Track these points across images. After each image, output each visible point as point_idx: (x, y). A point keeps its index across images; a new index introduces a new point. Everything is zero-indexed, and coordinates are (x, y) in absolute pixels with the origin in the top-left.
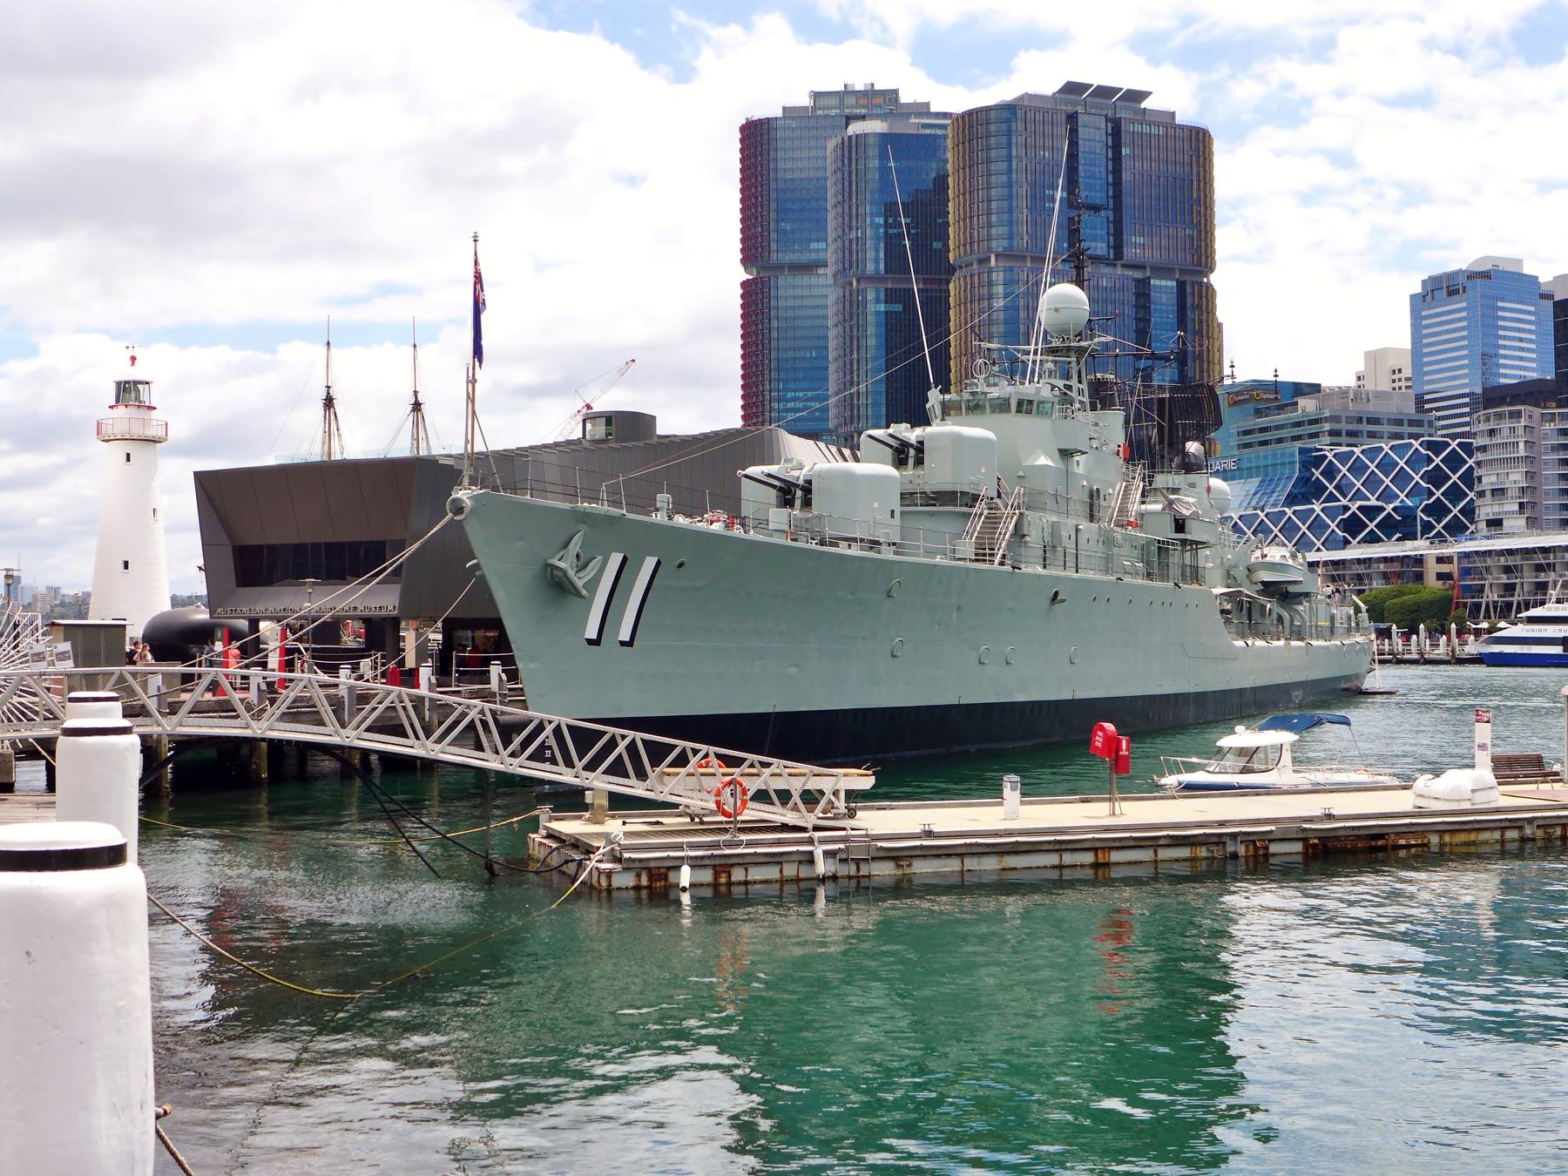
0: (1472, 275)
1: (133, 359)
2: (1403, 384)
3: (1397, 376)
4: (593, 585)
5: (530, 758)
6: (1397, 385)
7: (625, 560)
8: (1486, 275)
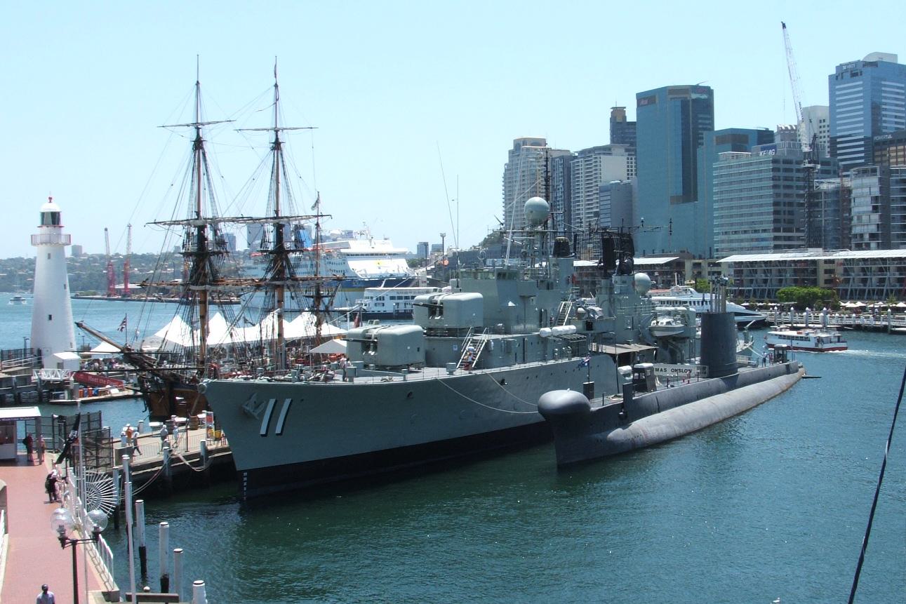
0: (866, 64)
2: (826, 129)
3: (822, 124)
4: (262, 415)
6: (822, 129)
8: (873, 64)
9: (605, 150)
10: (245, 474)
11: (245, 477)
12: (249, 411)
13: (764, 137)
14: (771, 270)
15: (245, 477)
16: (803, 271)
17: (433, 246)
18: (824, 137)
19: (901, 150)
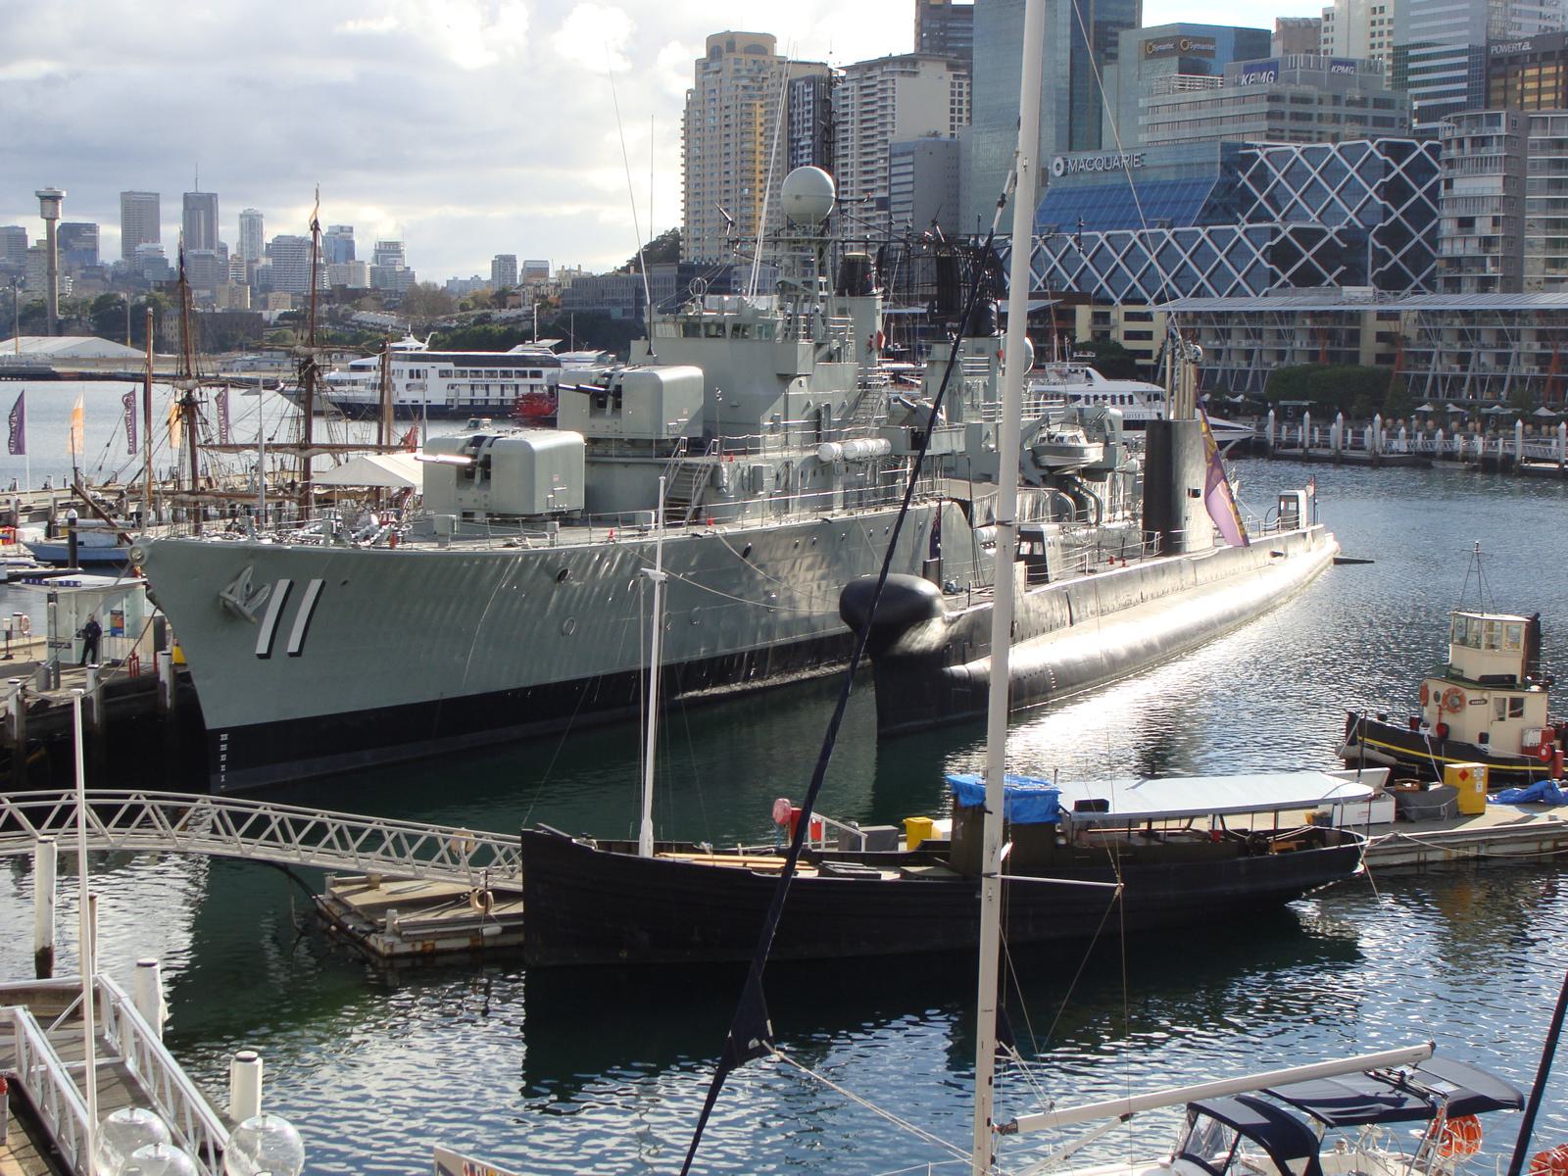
2: (1386, 28)
3: (1377, 17)
4: (261, 612)
9: (904, 64)
10: (224, 737)
11: (224, 742)
12: (235, 605)
13: (1250, 44)
14: (1479, 331)
15: (224, 742)
16: (1331, 335)
17: (525, 262)
18: (1381, 45)
19: (1548, 77)
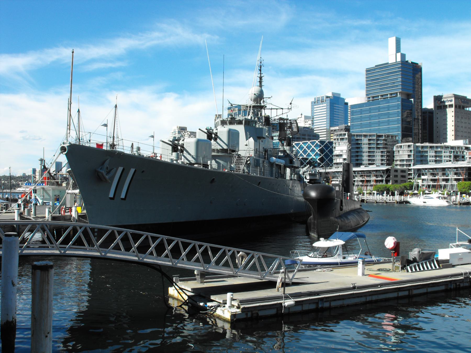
1: (291, 104)
4: (112, 178)
5: (74, 244)
7: (123, 170)
